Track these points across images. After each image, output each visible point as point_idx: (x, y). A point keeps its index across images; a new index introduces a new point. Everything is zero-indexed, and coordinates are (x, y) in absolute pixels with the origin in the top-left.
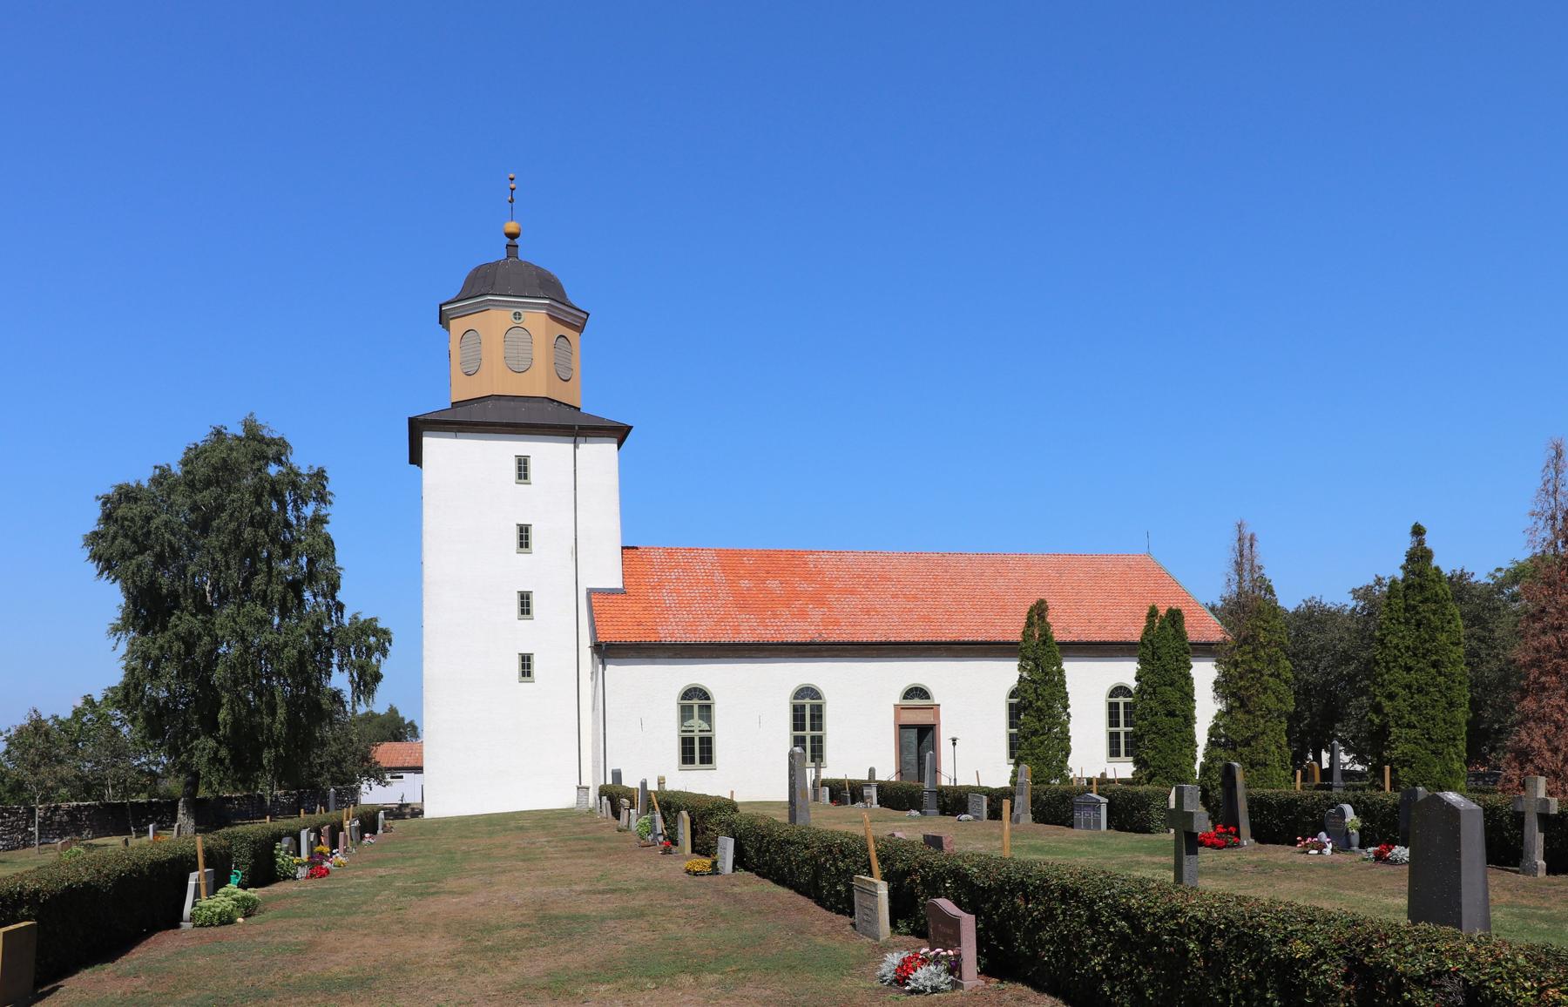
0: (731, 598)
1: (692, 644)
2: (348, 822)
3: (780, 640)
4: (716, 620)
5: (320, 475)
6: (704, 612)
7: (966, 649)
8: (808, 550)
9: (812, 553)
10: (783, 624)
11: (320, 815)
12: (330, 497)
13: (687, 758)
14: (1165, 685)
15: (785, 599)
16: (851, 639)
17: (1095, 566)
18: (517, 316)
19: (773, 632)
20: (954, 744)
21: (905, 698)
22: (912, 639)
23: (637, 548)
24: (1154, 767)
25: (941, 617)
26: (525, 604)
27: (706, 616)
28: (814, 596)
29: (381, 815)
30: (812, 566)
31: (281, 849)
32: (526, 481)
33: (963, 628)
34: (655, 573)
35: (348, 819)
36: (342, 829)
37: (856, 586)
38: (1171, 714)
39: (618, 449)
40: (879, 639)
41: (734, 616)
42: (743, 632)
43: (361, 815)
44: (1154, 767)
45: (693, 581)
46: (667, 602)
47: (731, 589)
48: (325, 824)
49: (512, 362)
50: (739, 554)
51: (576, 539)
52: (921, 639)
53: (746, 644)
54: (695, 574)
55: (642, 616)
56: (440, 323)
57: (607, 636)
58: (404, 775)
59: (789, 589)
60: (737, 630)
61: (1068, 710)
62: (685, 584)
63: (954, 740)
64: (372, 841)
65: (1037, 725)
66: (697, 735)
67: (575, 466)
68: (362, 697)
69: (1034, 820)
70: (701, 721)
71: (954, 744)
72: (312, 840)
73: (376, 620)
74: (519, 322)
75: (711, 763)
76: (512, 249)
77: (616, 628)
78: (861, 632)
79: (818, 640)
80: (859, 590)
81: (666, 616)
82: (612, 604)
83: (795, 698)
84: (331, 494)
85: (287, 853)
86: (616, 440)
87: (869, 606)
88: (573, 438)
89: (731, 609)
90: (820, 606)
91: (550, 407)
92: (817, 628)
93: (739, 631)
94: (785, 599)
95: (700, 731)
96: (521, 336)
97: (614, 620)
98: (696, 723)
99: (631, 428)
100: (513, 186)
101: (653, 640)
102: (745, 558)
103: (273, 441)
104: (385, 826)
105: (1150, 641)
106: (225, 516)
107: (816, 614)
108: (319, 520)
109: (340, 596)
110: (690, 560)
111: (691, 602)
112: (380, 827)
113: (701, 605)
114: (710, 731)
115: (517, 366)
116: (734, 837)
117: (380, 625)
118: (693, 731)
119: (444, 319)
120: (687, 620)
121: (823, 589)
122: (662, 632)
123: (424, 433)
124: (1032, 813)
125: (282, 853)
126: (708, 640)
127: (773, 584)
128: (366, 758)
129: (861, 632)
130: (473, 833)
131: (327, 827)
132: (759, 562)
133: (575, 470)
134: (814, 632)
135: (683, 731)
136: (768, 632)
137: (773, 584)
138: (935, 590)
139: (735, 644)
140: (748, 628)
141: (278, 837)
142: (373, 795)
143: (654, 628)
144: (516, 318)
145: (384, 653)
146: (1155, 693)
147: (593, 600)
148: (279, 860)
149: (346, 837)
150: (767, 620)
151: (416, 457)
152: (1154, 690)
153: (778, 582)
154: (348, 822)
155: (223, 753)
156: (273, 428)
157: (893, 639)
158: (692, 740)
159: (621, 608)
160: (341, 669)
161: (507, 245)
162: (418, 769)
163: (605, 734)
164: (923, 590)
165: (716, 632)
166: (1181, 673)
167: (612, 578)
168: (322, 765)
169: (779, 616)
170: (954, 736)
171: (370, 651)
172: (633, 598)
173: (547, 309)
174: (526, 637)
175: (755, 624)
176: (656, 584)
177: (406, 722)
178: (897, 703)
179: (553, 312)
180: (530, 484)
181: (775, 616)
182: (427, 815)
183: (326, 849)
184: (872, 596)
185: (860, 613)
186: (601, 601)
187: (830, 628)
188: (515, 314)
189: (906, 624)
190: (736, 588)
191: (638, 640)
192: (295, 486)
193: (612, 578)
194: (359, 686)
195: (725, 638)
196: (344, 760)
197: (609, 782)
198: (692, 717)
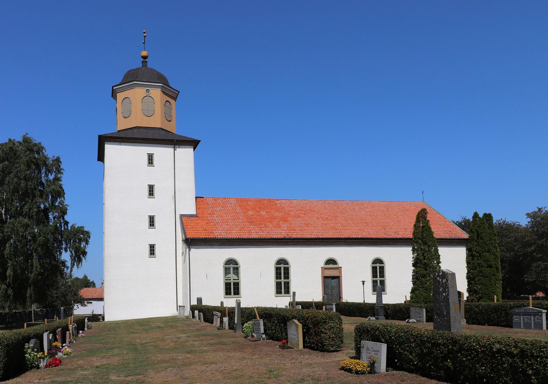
0: (245, 219)
1: (230, 239)
2: (71, 325)
3: (270, 237)
4: (240, 228)
5: (58, 161)
6: (234, 225)
7: (352, 241)
8: (277, 199)
9: (278, 200)
10: (270, 230)
11: (57, 321)
12: (62, 171)
13: (228, 292)
14: (485, 252)
15: (270, 219)
16: (302, 237)
17: (401, 206)
18: (148, 91)
19: (266, 233)
20: (363, 284)
21: (326, 264)
22: (329, 237)
23: (203, 198)
24: (481, 294)
25: (340, 227)
26: (152, 221)
27: (235, 227)
28: (282, 218)
29: (86, 320)
30: (279, 205)
31: (29, 348)
32: (152, 165)
33: (351, 232)
34: (210, 208)
35: (71, 324)
36: (68, 330)
37: (300, 214)
38: (490, 266)
39: (194, 151)
40: (314, 237)
41: (247, 227)
42: (253, 233)
43: (77, 321)
44: (481, 294)
45: (227, 212)
46: (217, 220)
47: (245, 215)
48: (58, 328)
49: (146, 112)
50: (247, 200)
51: (175, 192)
52: (333, 237)
53: (255, 239)
54: (228, 209)
55: (206, 227)
56: (112, 97)
57: (191, 235)
58: (93, 302)
59: (271, 215)
60: (250, 232)
61: (440, 264)
62: (224, 213)
63: (363, 282)
64: (83, 335)
65: (425, 272)
66: (232, 282)
67: (174, 158)
68: (75, 264)
69: (467, 322)
70: (234, 275)
71: (363, 284)
72: (50, 338)
73: (83, 227)
74: (149, 94)
75: (289, 294)
76: (144, 63)
77: (195, 232)
78: (306, 234)
79: (287, 237)
80: (301, 215)
81: (217, 227)
82: (192, 221)
83: (277, 264)
84: (62, 169)
85: (33, 351)
86: (193, 147)
87: (307, 223)
88: (173, 146)
89: (246, 224)
90: (285, 222)
91: (163, 132)
92: (286, 232)
93: (251, 233)
94: (270, 219)
95: (234, 280)
96: (149, 100)
97: (193, 228)
98: (232, 276)
99: (199, 141)
100: (145, 35)
101: (212, 237)
102: (249, 202)
103: (36, 145)
104: (88, 326)
105: (476, 230)
106: (12, 175)
107: (285, 226)
108: (57, 179)
109: (67, 218)
110: (225, 203)
111: (227, 220)
112: (86, 327)
113: (232, 222)
114: (238, 280)
115: (147, 114)
116: (386, 342)
117: (86, 229)
118: (230, 280)
119: (114, 95)
120: (227, 228)
121: (286, 215)
122: (216, 233)
123: (105, 143)
124: (465, 318)
125: (29, 351)
126: (237, 237)
127: (263, 213)
128: (76, 294)
129: (306, 234)
130: (136, 330)
131: (59, 329)
132: (255, 204)
133: (174, 160)
134: (285, 233)
135: (226, 280)
136: (264, 233)
137: (263, 213)
138: (335, 216)
139: (249, 239)
140: (254, 232)
141: (27, 339)
142: (79, 310)
143: (212, 232)
144: (147, 92)
145: (87, 243)
146: (480, 256)
147: (183, 220)
148: (27, 355)
149: (70, 334)
150: (263, 229)
151: (101, 157)
152: (480, 254)
153: (265, 212)
154: (71, 325)
155: (10, 292)
156: (36, 138)
157: (321, 237)
158: (230, 284)
159: (196, 223)
160: (66, 251)
161: (142, 62)
162: (102, 299)
163: (190, 281)
164: (329, 216)
165: (240, 233)
166: (493, 246)
167: (192, 211)
168: (57, 297)
169: (268, 227)
170: (363, 280)
171: (80, 240)
172: (201, 219)
173: (161, 88)
174: (152, 236)
175: (258, 230)
176: (211, 213)
177: (91, 281)
178: (323, 266)
179: (164, 90)
180: (154, 166)
181: (266, 226)
182: (106, 319)
183: (59, 344)
184: (308, 218)
185: (304, 226)
186: (187, 220)
187: (292, 232)
188: (147, 90)
189: (325, 230)
190: (247, 215)
191: (205, 237)
192: (45, 164)
193: (192, 211)
194: (75, 258)
195: (245, 236)
196: (67, 295)
197: (292, 301)
198: (230, 273)
